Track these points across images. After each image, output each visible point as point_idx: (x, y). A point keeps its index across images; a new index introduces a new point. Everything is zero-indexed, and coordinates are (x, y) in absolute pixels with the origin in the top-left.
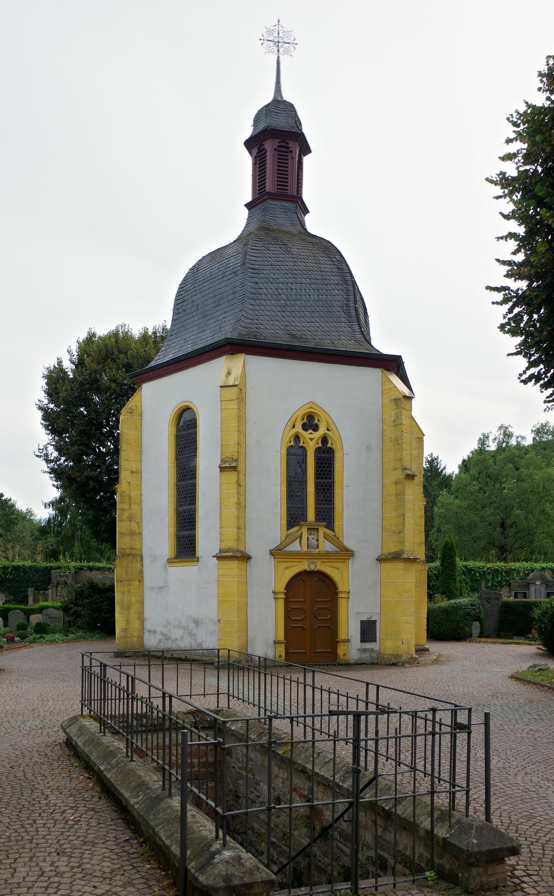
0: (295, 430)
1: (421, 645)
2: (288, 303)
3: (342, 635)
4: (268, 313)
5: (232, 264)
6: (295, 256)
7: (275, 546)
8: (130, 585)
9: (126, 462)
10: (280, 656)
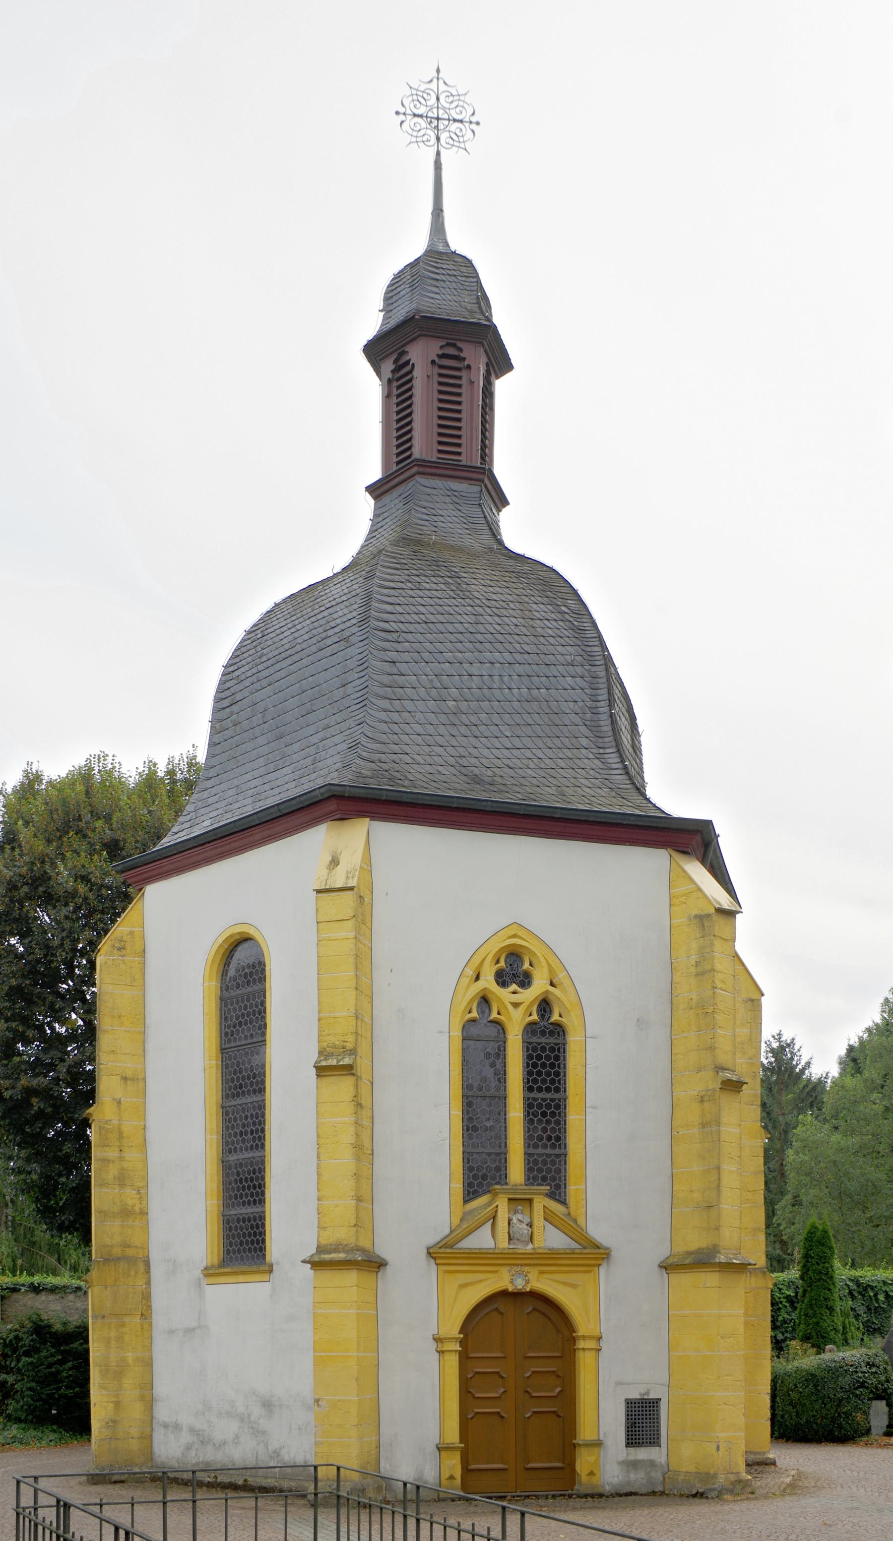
2: (464, 706)
3: (585, 1432)
5: (338, 621)
7: (438, 1239)
8: (123, 1325)
10: (452, 1477)
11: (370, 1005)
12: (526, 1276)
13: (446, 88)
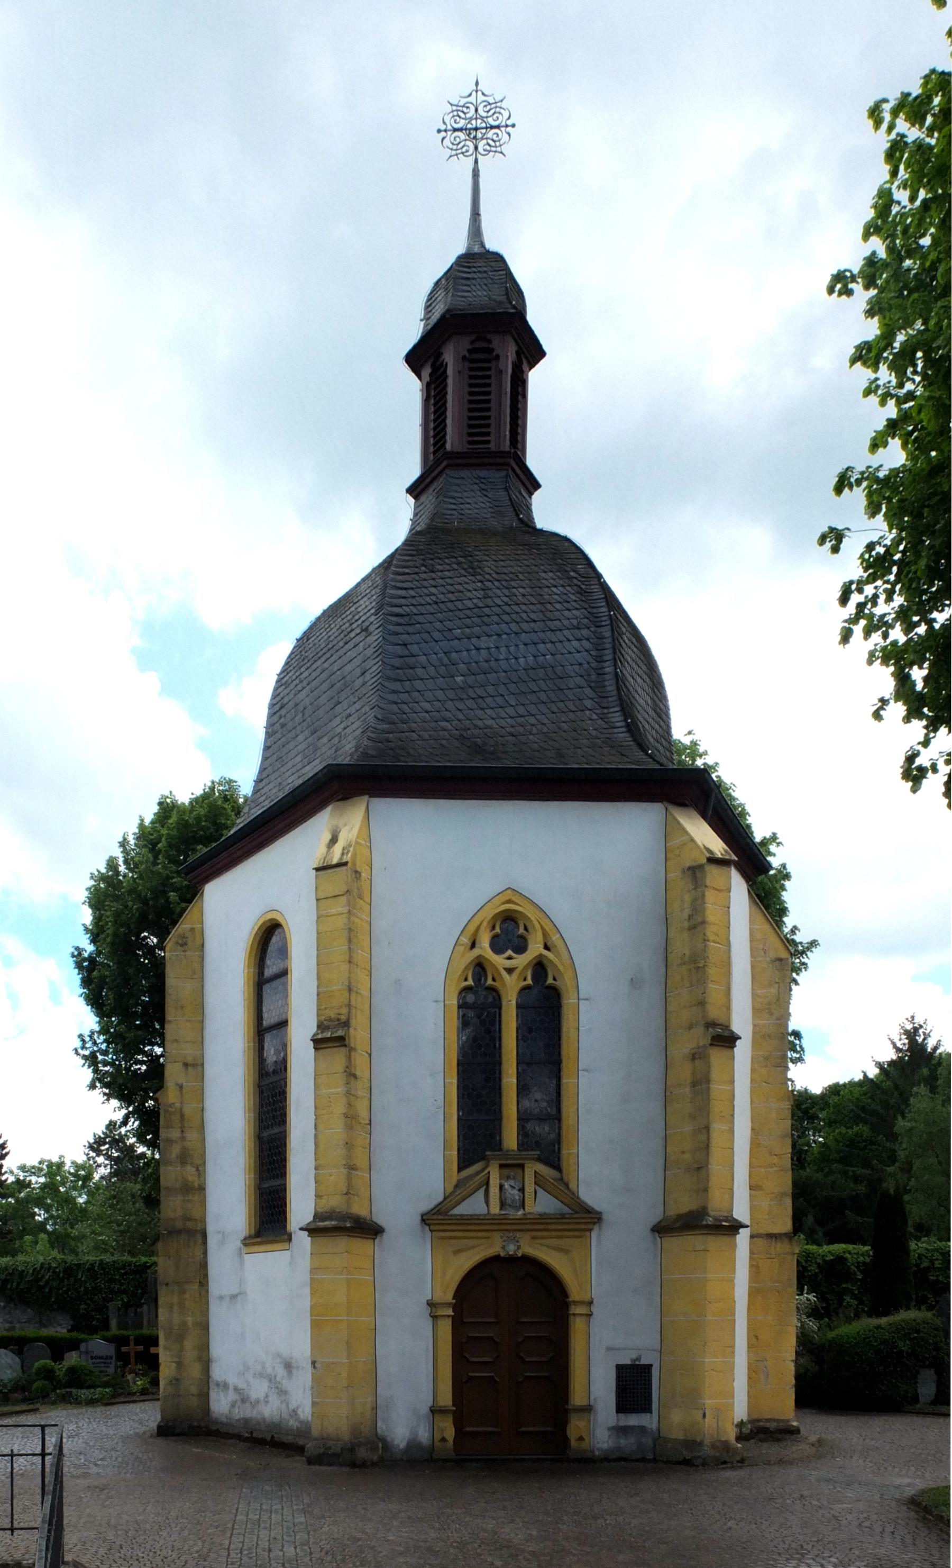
0: (476, 952)
1: (783, 1421)
3: (577, 1398)
5: (361, 614)
6: (487, 577)
7: (432, 1206)
8: (184, 1292)
9: (175, 1045)
11: (368, 978)
12: (518, 1242)
13: (485, 98)
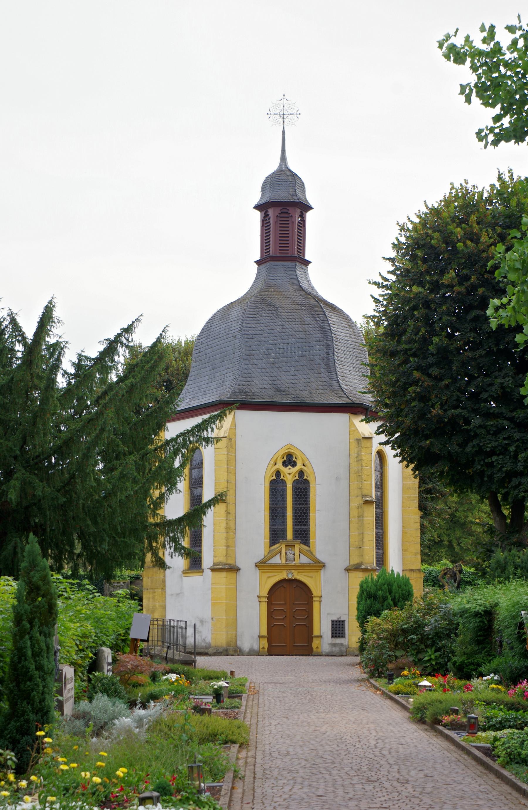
0: (277, 467)
2: (277, 360)
3: (316, 632)
4: (259, 370)
5: (233, 328)
6: (283, 320)
8: (155, 593)
10: (263, 648)
